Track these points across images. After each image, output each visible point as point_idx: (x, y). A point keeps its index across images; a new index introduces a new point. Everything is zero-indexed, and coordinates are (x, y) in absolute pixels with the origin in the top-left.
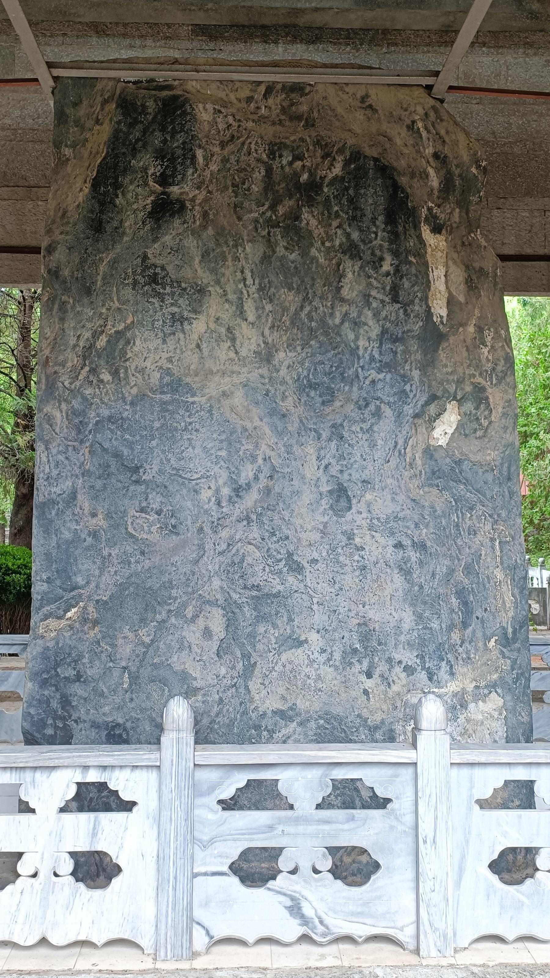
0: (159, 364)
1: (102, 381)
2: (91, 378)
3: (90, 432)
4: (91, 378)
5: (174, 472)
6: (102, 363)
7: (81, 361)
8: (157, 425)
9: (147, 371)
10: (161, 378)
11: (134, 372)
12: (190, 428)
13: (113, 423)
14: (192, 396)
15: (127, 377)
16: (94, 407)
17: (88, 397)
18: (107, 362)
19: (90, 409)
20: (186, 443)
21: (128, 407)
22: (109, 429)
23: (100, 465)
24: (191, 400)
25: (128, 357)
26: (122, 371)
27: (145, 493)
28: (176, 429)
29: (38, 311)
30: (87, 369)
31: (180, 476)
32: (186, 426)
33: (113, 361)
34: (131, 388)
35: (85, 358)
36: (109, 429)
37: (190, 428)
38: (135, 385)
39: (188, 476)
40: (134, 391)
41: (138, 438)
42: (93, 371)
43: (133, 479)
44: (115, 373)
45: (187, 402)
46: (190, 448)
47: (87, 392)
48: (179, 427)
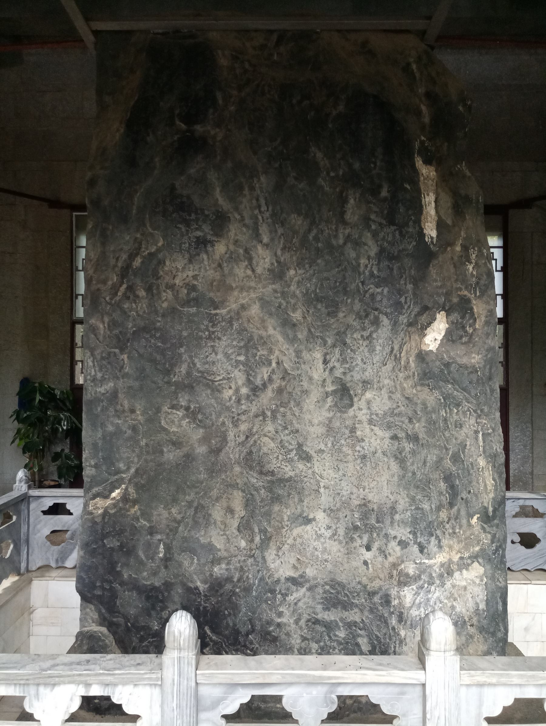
0: (187, 281)
1: (138, 297)
2: (128, 294)
3: (128, 341)
4: (128, 294)
5: (200, 375)
8: (185, 334)
9: (176, 288)
10: (188, 294)
11: (164, 288)
13: (147, 333)
14: (215, 309)
15: (159, 293)
16: (131, 319)
20: (210, 350)
22: (144, 338)
24: (213, 312)
26: (155, 287)
28: (201, 338)
30: (125, 286)
31: (205, 378)
32: (209, 335)
34: (163, 302)
36: (144, 338)
37: (213, 336)
38: (166, 300)
39: (211, 378)
40: (165, 305)
41: (168, 345)
42: (130, 288)
43: (165, 380)
44: (149, 289)
45: (211, 314)
46: (214, 354)
48: (204, 336)
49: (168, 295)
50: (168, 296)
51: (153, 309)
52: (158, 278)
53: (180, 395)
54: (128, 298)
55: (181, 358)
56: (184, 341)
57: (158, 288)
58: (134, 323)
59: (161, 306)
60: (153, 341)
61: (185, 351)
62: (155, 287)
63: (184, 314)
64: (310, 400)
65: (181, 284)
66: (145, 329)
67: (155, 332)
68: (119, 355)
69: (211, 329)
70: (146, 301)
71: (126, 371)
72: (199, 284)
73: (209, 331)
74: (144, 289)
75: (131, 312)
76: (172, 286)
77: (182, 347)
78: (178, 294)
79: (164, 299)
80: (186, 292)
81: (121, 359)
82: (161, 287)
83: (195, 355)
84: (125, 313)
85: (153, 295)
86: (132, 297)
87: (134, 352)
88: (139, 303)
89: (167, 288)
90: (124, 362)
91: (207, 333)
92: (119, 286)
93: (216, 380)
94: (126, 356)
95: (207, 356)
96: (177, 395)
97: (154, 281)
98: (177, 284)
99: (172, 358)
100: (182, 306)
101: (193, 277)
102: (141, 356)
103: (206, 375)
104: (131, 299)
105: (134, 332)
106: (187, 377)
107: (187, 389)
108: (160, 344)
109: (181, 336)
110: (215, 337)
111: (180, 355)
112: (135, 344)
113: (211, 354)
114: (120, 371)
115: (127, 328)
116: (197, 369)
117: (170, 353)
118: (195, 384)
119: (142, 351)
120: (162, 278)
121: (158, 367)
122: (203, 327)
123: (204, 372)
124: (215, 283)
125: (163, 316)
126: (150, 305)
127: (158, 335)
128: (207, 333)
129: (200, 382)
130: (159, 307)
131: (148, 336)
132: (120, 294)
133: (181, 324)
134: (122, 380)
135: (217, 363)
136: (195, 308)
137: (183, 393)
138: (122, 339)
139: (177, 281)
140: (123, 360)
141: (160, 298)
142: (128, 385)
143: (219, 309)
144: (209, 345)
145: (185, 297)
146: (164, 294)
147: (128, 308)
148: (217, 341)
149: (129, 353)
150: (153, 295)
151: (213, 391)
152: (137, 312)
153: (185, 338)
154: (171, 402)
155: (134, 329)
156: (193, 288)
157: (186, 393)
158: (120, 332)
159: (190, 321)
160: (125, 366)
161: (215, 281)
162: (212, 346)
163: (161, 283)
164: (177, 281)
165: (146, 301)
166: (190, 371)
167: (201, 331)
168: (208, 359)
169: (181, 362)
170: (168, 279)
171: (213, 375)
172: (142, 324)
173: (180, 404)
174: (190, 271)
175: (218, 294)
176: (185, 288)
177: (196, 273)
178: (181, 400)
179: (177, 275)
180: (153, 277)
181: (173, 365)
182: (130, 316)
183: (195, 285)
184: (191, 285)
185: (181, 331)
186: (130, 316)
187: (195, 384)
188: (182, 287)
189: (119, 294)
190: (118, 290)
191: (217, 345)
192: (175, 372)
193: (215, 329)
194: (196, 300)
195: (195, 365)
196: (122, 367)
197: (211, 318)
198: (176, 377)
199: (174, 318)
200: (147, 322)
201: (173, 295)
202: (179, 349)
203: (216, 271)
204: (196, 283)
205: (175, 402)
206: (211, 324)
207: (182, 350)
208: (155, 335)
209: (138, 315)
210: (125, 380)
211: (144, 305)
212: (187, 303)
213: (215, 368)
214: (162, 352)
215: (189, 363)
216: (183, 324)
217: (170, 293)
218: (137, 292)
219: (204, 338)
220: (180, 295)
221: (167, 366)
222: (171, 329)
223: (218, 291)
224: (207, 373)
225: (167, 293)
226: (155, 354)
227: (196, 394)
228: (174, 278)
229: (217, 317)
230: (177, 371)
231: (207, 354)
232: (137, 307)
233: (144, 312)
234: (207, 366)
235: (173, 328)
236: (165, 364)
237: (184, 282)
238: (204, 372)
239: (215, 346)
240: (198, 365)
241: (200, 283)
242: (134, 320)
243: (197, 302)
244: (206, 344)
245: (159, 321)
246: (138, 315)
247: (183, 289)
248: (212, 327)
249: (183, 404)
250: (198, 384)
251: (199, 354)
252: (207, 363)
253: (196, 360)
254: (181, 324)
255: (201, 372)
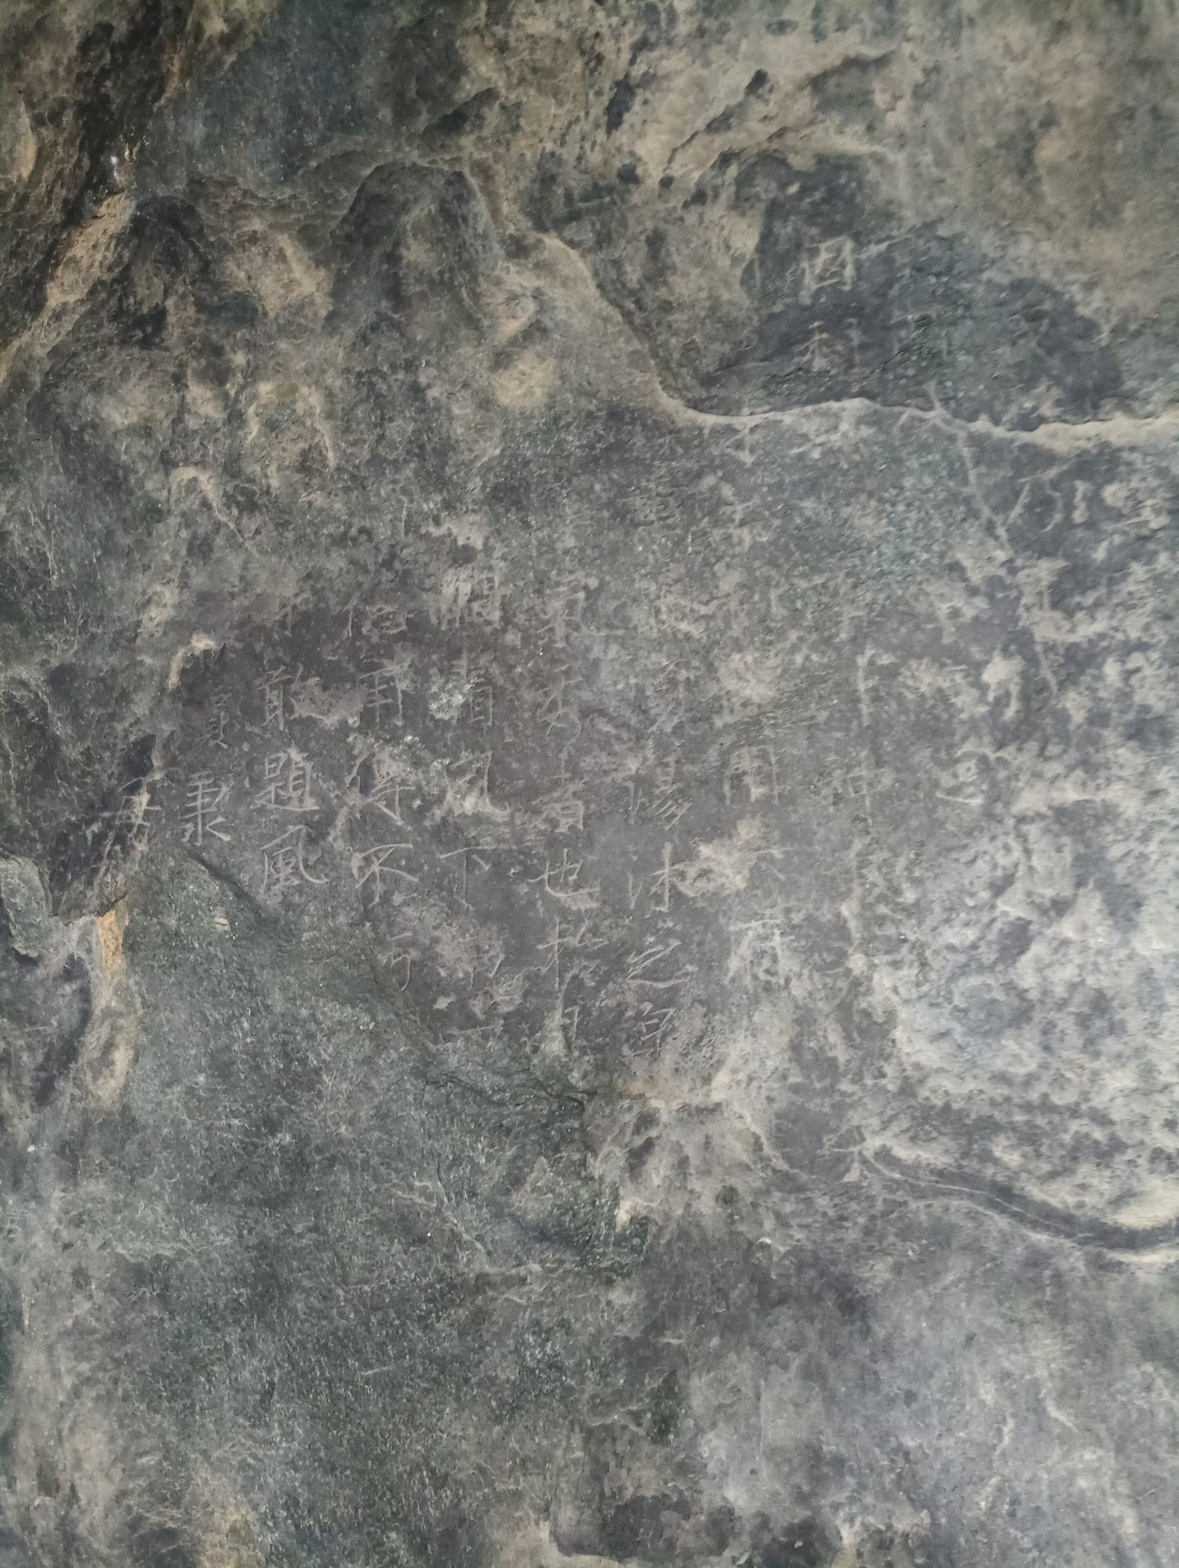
0: (753, 133)
1: (244, 311)
2: (148, 288)
3: (136, 763)
4: (148, 288)
5: (934, 1155)
6: (251, 166)
7: (68, 158)
8: (749, 680)
9: (643, 209)
10: (774, 257)
11: (517, 223)
12: (1075, 705)
13: (332, 678)
14: (1085, 400)
15: (460, 274)
16: (169, 539)
17: (127, 450)
18: (291, 160)
19: (135, 558)
20: (1048, 864)
21: (468, 530)
22: (302, 731)
23: (222, 1069)
24: (1065, 436)
25: (468, 88)
26: (422, 210)
27: (640, 1355)
28: (935, 726)
29: (1009, 1426)
30: (115, 214)
31: (1004, 1196)
32: (1033, 691)
33: (340, 144)
34: (501, 359)
35: (97, 127)
36: (302, 731)
37: (1075, 705)
38: (535, 331)
39: (1084, 1191)
40: (526, 386)
41: (567, 813)
42: (171, 233)
43: (530, 1203)
44: (358, 239)
45: (1041, 457)
46: (1091, 905)
47: (118, 414)
48: (967, 703)
49: (564, 282)
50: (556, 294)
51: (400, 428)
52: (455, 121)
53: (699, 1391)
54: (145, 329)
55: (712, 963)
56: (745, 761)
57: (451, 216)
58: (199, 579)
59: (485, 403)
60: (391, 767)
61: (757, 877)
62: (422, 210)
63: (731, 471)
64: (317, 692)
65: (690, 170)
66: (310, 643)
67: (420, 673)
68: (42, 917)
69: (1047, 628)
70: (334, 349)
71: (107, 1090)
72: (901, 159)
73: (1019, 643)
74: (307, 236)
75: (167, 463)
76: (597, 191)
77: (718, 829)
78: (658, 271)
79: (511, 327)
80: (745, 237)
81: (56, 962)
82: (480, 206)
83: (872, 920)
84: (115, 481)
85: (396, 294)
86: (180, 317)
87: (200, 886)
88: (253, 374)
89: (541, 213)
90: (85, 994)
91: (1000, 671)
92: (55, 214)
93: (1132, 1218)
94: (107, 930)
95: (1017, 939)
96: (671, 1390)
97: (414, 156)
98: (653, 174)
99: (613, 961)
100: (713, 384)
101: (816, 83)
102: (260, 925)
103: (1007, 1154)
104: (173, 334)
105: (201, 678)
106: (786, 1183)
107: (785, 1321)
108: (469, 804)
109: (702, 714)
110: (1098, 718)
111: (701, 919)
112: (211, 798)
113: (1060, 907)
114: (44, 1094)
115: (127, 639)
116: (907, 1089)
117: (582, 901)
118: (879, 1272)
119: (273, 880)
120: (492, 116)
121: (456, 1054)
122: (948, 603)
123: (988, 1127)
124: (1050, 149)
125: (509, 495)
126: (370, 395)
127: (449, 700)
128: (1000, 671)
129: (941, 1237)
130: (463, 409)
131: (340, 714)
132: (64, 292)
133: (699, 579)
134: (56, 1197)
135: (1134, 1020)
136: (854, 406)
137: (741, 1367)
138: (72, 752)
139: (650, 144)
140: (73, 970)
141: (472, 321)
142: (132, 1248)
143: (1126, 402)
144: (1031, 799)
145: (737, 298)
146: (517, 278)
147: (145, 430)
148: (1127, 757)
149: (150, 897)
150: (396, 294)
151: (1096, 1345)
152: (231, 467)
153: (750, 729)
154: (599, 1471)
155: (202, 643)
156: (833, 196)
157: (768, 1360)
158: (60, 679)
159: (809, 547)
160: (93, 1041)
161: (1048, 122)
162: (1065, 818)
163: (484, 171)
164: (650, 144)
165: (334, 349)
166: (820, 1106)
167: (943, 655)
168: (1026, 974)
169: (709, 1006)
170: (552, 126)
171: (1105, 1154)
172: (282, 587)
173: (709, 1498)
174: (782, 28)
175: (1109, 248)
176: (740, 203)
177: (850, 43)
178: (715, 1447)
179: (648, 80)
180: (404, 111)
181: (613, 1041)
182: (155, 513)
183: (849, 164)
184: (798, 162)
185: (707, 656)
186: (155, 513)
187: (879, 1272)
188: (699, 197)
189: (55, 296)
190: (52, 257)
191: (1130, 806)
192: (647, 1120)
193: (1086, 630)
194: (857, 315)
195: (870, 1032)
196: (64, 1054)
197: (1041, 505)
198: (658, 1169)
199: (622, 516)
200: (335, 563)
201: (611, 287)
202: (684, 854)
203: (1061, 28)
204: (849, 141)
205: (643, 1478)
206: (1045, 570)
207: (724, 865)
208: (416, 704)
209: (247, 500)
210: (96, 1187)
211: (311, 399)
212: (772, 349)
213: (1119, 1080)
214: (501, 894)
215: (804, 1020)
216: (729, 581)
217: (577, 265)
218: (237, 271)
219: (974, 726)
220: (686, 285)
221: (554, 1046)
222: (591, 633)
223: (1103, 216)
224: (1029, 1138)
225: (541, 267)
226: (418, 917)
227: (894, 1382)
228: (614, 117)
229: (1113, 493)
230: (663, 1107)
231: (1012, 907)
232: (236, 418)
233: (307, 464)
234: (1018, 1053)
235: (618, 625)
236: (524, 1023)
237: (720, 142)
238: (988, 1127)
239: (1108, 814)
240: (915, 1044)
241: (902, 140)
242: (201, 549)
243: (875, 335)
244: (999, 796)
245: (462, 556)
246: (247, 500)
247: (716, 211)
248: (1059, 597)
249: (737, 1496)
250: (924, 1270)
251: (916, 911)
252: (1022, 1013)
253: (887, 985)
254: (699, 579)
255: (931, 1119)
